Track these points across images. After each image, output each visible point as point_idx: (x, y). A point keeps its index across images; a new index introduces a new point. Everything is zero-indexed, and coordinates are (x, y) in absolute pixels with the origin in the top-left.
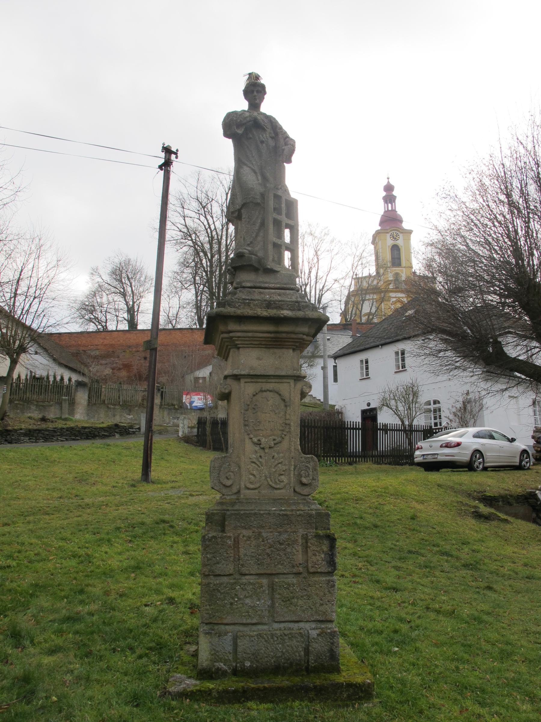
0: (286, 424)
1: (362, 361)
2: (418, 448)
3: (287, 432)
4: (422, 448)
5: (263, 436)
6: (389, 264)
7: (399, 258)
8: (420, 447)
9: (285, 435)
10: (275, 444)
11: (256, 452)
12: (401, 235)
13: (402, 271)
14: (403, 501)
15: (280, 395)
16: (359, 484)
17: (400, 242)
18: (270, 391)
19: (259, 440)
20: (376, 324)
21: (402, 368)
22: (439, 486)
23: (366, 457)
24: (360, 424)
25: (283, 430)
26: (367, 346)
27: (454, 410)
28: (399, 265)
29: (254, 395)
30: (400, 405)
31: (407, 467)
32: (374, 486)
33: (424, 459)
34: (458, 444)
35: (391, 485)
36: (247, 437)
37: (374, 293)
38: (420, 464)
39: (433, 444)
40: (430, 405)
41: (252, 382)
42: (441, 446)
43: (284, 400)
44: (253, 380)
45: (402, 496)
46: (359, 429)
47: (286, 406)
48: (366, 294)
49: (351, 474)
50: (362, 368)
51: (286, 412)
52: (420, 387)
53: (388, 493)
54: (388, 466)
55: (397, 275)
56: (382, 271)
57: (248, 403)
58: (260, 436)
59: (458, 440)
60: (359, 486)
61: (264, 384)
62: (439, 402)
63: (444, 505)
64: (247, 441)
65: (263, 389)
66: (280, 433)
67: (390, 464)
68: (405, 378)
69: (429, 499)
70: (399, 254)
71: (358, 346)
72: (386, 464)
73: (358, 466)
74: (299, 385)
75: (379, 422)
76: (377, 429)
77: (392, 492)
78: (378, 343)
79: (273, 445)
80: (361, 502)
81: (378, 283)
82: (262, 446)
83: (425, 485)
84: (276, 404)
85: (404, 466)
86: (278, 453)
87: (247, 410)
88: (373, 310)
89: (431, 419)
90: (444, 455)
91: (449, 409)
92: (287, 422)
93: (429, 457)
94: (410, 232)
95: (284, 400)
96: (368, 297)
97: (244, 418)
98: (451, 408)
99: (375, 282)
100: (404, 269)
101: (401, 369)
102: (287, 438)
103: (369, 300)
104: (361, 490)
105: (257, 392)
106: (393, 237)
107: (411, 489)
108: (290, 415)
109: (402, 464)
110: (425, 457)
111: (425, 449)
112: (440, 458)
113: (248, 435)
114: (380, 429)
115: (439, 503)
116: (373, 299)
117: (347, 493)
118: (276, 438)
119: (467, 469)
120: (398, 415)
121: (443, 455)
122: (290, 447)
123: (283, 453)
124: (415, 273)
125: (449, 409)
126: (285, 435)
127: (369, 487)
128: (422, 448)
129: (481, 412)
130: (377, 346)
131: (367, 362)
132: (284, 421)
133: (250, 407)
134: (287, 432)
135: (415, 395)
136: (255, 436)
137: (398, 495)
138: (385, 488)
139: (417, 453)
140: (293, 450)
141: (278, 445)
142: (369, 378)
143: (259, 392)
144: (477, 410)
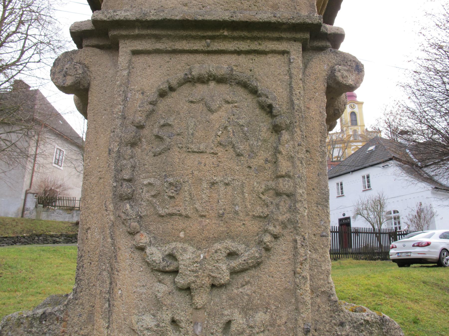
0: (278, 194)
1: (338, 184)
2: (393, 247)
3: (284, 225)
4: (396, 247)
5: (189, 240)
6: (350, 124)
7: (356, 120)
8: (394, 246)
9: (276, 237)
10: (234, 272)
11: (158, 304)
12: (356, 105)
13: (358, 129)
14: (399, 300)
15: (254, 92)
16: (352, 282)
17: (356, 110)
18: (220, 80)
19: (172, 256)
20: (343, 161)
21: (368, 187)
22: (424, 282)
23: (347, 254)
24: (338, 228)
25: (264, 218)
26: (341, 173)
27: (411, 217)
28: (356, 124)
29: (162, 94)
30: (370, 213)
31: (379, 262)
32: (366, 285)
33: (398, 256)
34: (428, 244)
35: (382, 284)
36: (124, 244)
37: (340, 143)
38: (394, 261)
39: (406, 244)
40: (391, 214)
41: (158, 52)
42: (413, 246)
43: (269, 109)
44: (159, 46)
45: (395, 295)
46: (336, 232)
47: (276, 129)
48: (335, 144)
49: (337, 268)
50: (338, 189)
51: (277, 151)
52: (385, 201)
53: (382, 292)
54: (364, 261)
55: (355, 131)
56: (345, 129)
57: (139, 118)
58: (178, 239)
59: (426, 240)
60: (353, 284)
61: (199, 57)
62: (398, 212)
63: (438, 305)
64: (126, 257)
65: (195, 73)
66: (254, 227)
67: (366, 259)
68: (373, 194)
69: (421, 298)
70: (356, 118)
71: (335, 173)
72: (363, 259)
73: (341, 261)
74: (321, 65)
75: (352, 227)
76: (351, 232)
77: (385, 291)
78: (349, 170)
79: (225, 277)
80: (358, 302)
81: (342, 137)
82: (181, 281)
83: (413, 282)
84: (241, 122)
85: (377, 261)
86: (247, 309)
87: (133, 145)
88: (341, 154)
89: (392, 225)
90: (416, 253)
91: (406, 216)
92: (285, 185)
93: (403, 254)
94: (362, 103)
95: (269, 109)
96: (336, 146)
97: (119, 171)
98: (408, 216)
99: (341, 136)
100: (359, 127)
101: (367, 188)
102: (282, 247)
103: (337, 147)
104: (355, 288)
105: (174, 83)
106: (351, 107)
107: (401, 287)
108: (291, 158)
109: (375, 260)
110: (399, 254)
111: (399, 248)
112: (413, 256)
113: (132, 234)
114: (353, 232)
115: (433, 302)
116: (340, 147)
117: (343, 292)
118: (241, 248)
119: (436, 264)
120: (370, 222)
121: (415, 253)
122: (297, 286)
123: (267, 308)
124: (366, 129)
125: (406, 216)
126: (276, 237)
127: (362, 285)
128: (396, 247)
129: (432, 219)
130: (349, 173)
131: (341, 184)
132: (272, 184)
133: (146, 132)
134: (284, 225)
135: (381, 206)
136: (158, 240)
137: (391, 293)
138: (377, 286)
139: (392, 251)
140: (308, 299)
141: (246, 277)
142: (343, 196)
143: (181, 84)
144: (430, 217)
